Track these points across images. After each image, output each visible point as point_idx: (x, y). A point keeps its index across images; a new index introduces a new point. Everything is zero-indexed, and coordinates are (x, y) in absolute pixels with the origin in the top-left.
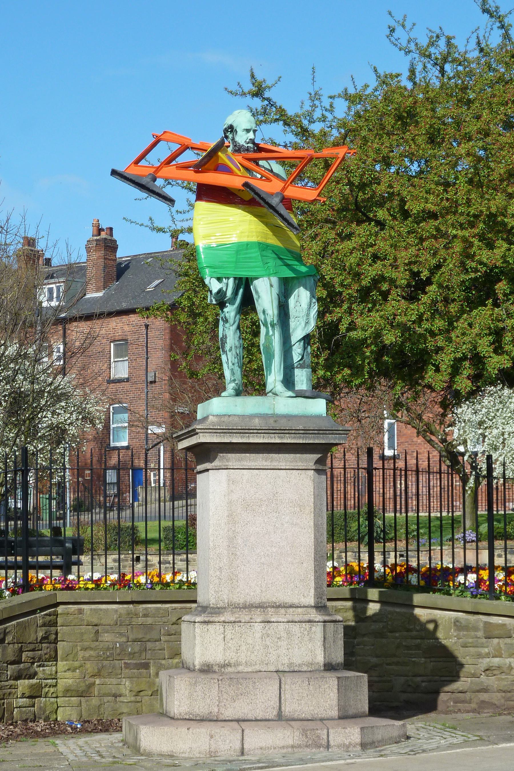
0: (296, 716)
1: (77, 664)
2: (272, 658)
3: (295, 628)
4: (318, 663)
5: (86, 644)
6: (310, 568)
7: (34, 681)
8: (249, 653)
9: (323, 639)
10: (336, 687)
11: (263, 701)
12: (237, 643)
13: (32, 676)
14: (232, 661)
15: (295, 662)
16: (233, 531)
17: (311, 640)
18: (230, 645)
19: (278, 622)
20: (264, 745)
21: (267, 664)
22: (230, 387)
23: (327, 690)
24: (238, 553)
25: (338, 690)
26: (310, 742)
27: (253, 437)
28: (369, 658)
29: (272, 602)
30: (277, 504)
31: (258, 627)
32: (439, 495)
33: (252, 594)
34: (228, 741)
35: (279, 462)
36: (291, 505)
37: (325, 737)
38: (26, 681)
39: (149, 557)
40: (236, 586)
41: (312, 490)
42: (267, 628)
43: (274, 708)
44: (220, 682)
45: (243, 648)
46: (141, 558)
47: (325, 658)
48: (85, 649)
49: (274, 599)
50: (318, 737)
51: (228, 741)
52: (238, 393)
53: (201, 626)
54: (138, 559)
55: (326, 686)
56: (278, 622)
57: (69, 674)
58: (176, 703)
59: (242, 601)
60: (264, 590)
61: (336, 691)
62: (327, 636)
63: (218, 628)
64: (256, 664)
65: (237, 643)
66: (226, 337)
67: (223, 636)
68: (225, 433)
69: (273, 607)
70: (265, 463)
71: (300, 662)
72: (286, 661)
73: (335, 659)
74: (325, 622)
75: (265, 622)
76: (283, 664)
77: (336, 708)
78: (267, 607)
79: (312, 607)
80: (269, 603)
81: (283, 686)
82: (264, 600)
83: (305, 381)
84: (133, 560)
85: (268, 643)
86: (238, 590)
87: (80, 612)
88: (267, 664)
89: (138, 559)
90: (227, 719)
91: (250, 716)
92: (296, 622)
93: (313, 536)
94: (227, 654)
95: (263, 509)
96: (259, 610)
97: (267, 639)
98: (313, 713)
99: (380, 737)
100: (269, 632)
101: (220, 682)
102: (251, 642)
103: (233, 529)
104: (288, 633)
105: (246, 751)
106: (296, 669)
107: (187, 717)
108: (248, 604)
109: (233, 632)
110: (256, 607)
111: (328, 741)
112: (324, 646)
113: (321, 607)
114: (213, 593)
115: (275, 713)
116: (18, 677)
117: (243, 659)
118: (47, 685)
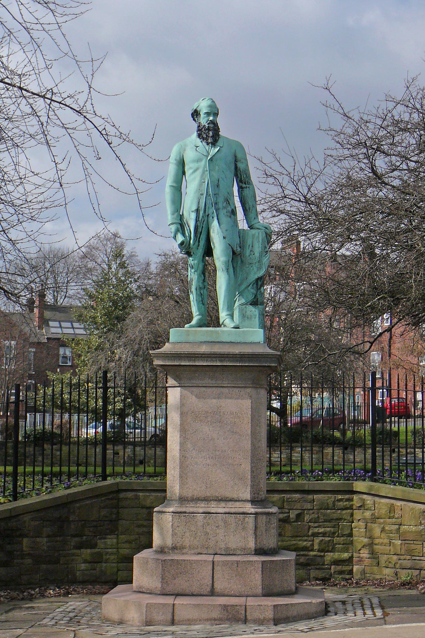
0: (226, 593)
1: (133, 537)
2: (212, 543)
3: (231, 519)
4: (250, 548)
5: (141, 522)
6: (247, 468)
7: (97, 550)
9: (254, 528)
10: (261, 569)
11: (199, 579)
13: (94, 546)
15: (230, 546)
17: (244, 529)
19: (217, 513)
20: (191, 618)
21: (207, 548)
22: (194, 322)
23: (253, 571)
24: (187, 456)
25: (262, 571)
26: (230, 616)
27: (199, 360)
28: (362, 539)
29: (216, 496)
30: (220, 416)
31: (200, 517)
33: (199, 489)
35: (223, 381)
36: (232, 416)
37: (243, 612)
38: (89, 551)
39: (401, 450)
41: (250, 404)
42: (207, 518)
43: (207, 585)
44: (163, 562)
45: (187, 534)
46: (396, 450)
47: (256, 544)
48: (139, 526)
49: (217, 494)
50: (237, 612)
52: (200, 325)
54: (394, 451)
55: (252, 568)
56: (217, 513)
57: (127, 545)
60: (208, 486)
61: (261, 573)
62: (258, 526)
64: (198, 548)
66: (192, 281)
68: (175, 357)
69: (216, 500)
70: (213, 382)
71: (234, 547)
72: (223, 546)
73: (267, 545)
74: (256, 514)
75: (206, 513)
77: (260, 587)
78: (211, 500)
79: (248, 501)
80: (213, 497)
81: (215, 567)
83: (258, 316)
84: (390, 451)
85: (208, 531)
87: (137, 498)
88: (207, 548)
89: (394, 451)
90: (168, 593)
91: (187, 592)
92: (232, 514)
93: (250, 442)
94: (174, 539)
95: (209, 420)
96: (204, 502)
97: (207, 527)
98: (240, 590)
99: (295, 613)
100: (209, 521)
102: (194, 529)
104: (225, 522)
105: (176, 621)
110: (202, 500)
111: (246, 616)
112: (255, 534)
113: (257, 501)
115: (209, 589)
116: (80, 546)
117: (187, 543)
118: (108, 553)
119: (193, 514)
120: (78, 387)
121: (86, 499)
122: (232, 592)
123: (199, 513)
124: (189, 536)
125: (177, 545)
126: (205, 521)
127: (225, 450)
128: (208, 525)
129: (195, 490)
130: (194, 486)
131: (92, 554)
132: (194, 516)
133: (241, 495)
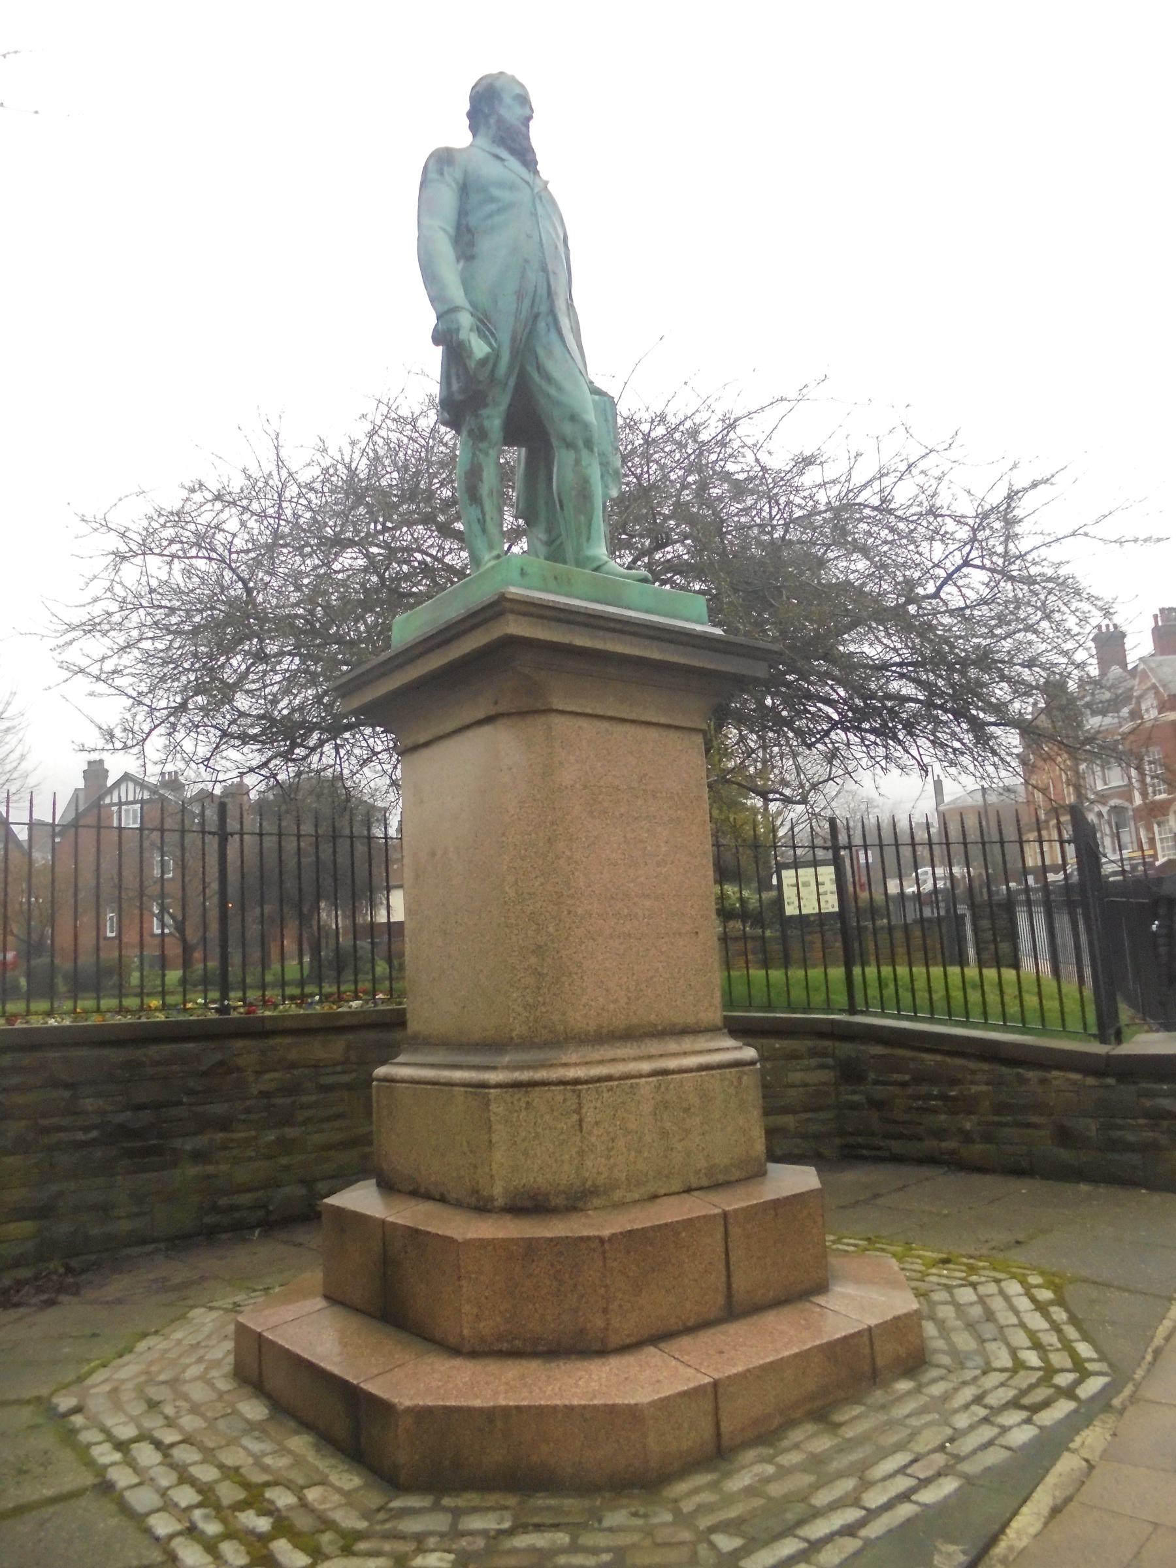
8: (633, 1153)
12: (608, 1133)
14: (600, 1181)
16: (569, 858)
18: (593, 1139)
21: (667, 1176)
31: (646, 1086)
32: (215, 886)
33: (612, 1006)
34: (686, 1425)
40: (579, 991)
45: (621, 1143)
51: (686, 1425)
53: (507, 1097)
58: (466, 1308)
59: (592, 1027)
63: (560, 1098)
65: (608, 1133)
67: (575, 1117)
72: (702, 1164)
76: (697, 1172)
82: (635, 1021)
85: (668, 1125)
86: (584, 999)
90: (628, 1341)
100: (667, 1097)
101: (607, 1246)
103: (568, 853)
106: (721, 1178)
107: (505, 1346)
108: (604, 1031)
109: (598, 1105)
114: (521, 1010)
115: (721, 1300)
119: (629, 1082)
120: (12, 798)
121: (876, 945)
122: (771, 1293)
123: (641, 1076)
124: (624, 1150)
125: (598, 1183)
126: (659, 1098)
127: (663, 894)
128: (666, 1108)
129: (603, 1009)
130: (601, 999)
131: (808, 1288)
132: (632, 1086)
133: (702, 1015)
